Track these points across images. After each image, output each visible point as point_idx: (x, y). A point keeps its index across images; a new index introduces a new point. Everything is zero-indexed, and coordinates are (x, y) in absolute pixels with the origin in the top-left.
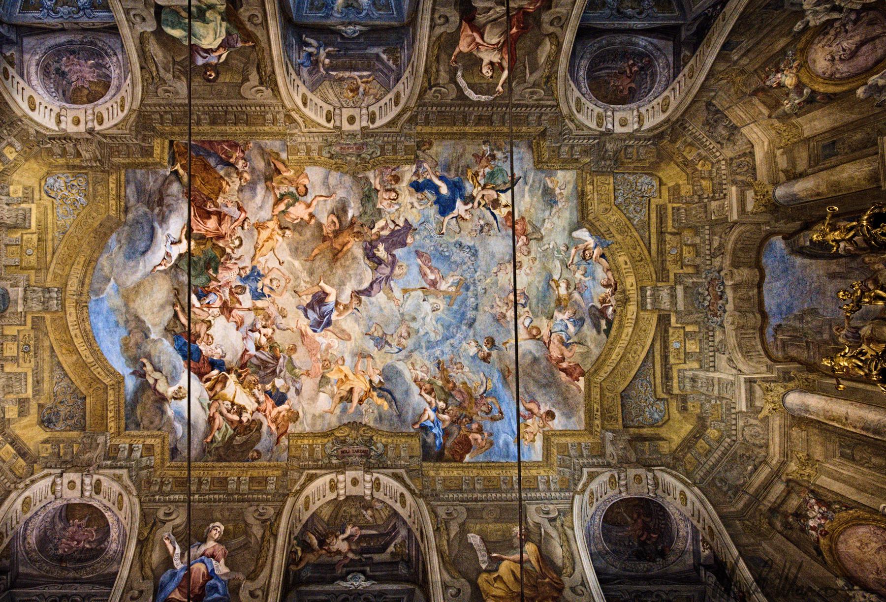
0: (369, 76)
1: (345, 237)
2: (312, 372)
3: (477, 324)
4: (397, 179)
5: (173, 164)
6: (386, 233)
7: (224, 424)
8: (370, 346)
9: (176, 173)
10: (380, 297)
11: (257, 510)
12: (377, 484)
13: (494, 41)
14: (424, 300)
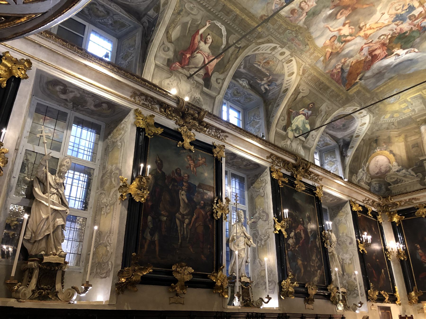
0: (256, 64)
5: (357, 82)
9: (360, 79)
13: (199, 55)
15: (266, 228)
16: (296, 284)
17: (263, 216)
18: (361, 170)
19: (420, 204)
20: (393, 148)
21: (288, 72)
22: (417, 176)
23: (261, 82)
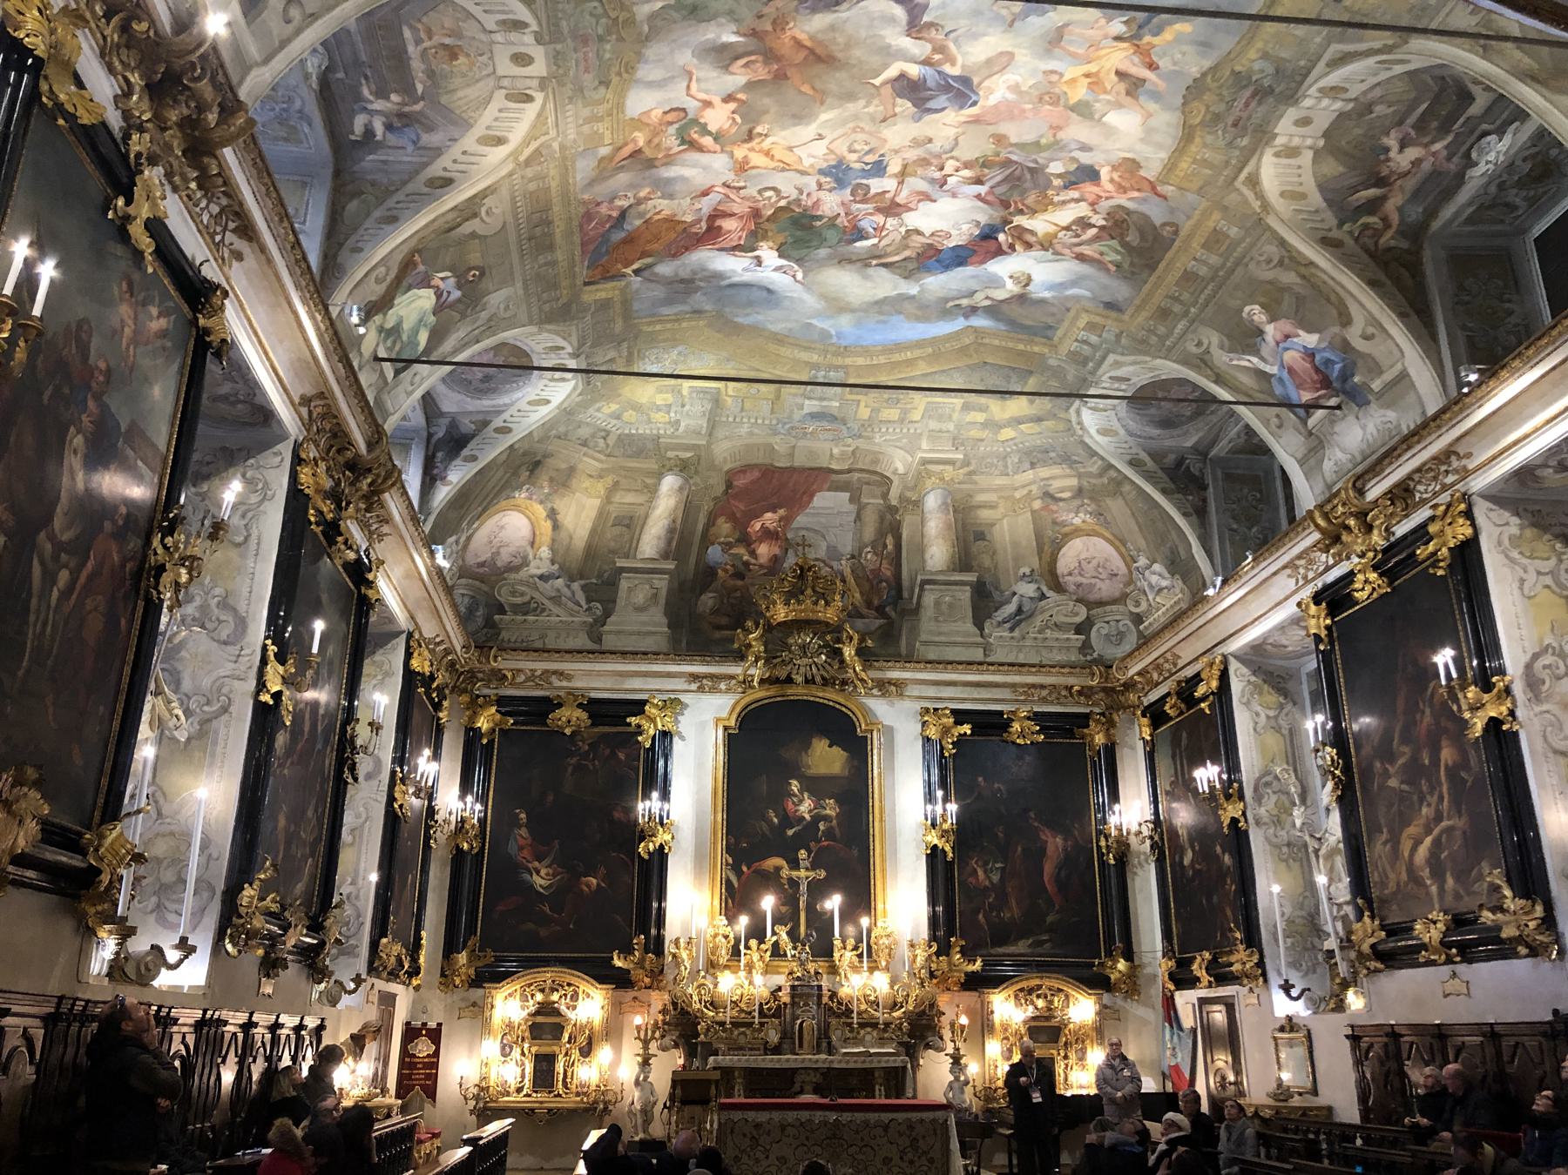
0: (411, 27)
1: (783, 44)
2: (1055, 122)
5: (624, 275)
7: (1096, 246)
9: (637, 272)
11: (1258, 262)
12: (1334, 92)
15: (222, 672)
16: (273, 901)
17: (220, 622)
18: (453, 538)
19: (569, 693)
20: (560, 504)
21: (488, 128)
22: (589, 609)
23: (371, 98)
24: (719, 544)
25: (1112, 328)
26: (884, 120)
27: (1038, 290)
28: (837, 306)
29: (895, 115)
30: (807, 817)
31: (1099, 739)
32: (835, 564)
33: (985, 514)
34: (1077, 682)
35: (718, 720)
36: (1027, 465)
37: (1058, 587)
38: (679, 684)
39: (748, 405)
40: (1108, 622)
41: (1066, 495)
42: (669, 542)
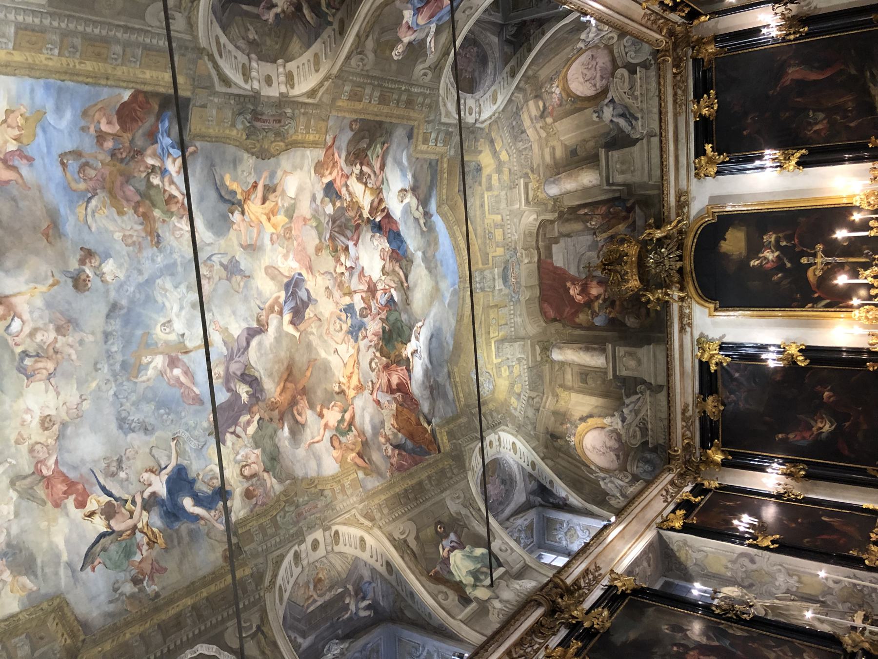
0: (308, 607)
1: (284, 399)
3: (104, 310)
4: (248, 494)
5: (432, 430)
6: (244, 418)
7: (373, 162)
8: (244, 263)
9: (429, 423)
10: (237, 329)
11: (364, 65)
12: (246, 74)
14: (183, 335)
18: (601, 483)
22: (641, 392)
24: (593, 318)
25: (424, 128)
26: (320, 320)
27: (408, 181)
28: (435, 293)
29: (315, 315)
30: (777, 254)
31: (711, 48)
32: (600, 245)
33: (559, 153)
34: (670, 71)
35: (710, 315)
36: (524, 135)
37: (604, 92)
38: (687, 339)
39: (503, 322)
40: (626, 53)
41: (541, 104)
42: (594, 349)
